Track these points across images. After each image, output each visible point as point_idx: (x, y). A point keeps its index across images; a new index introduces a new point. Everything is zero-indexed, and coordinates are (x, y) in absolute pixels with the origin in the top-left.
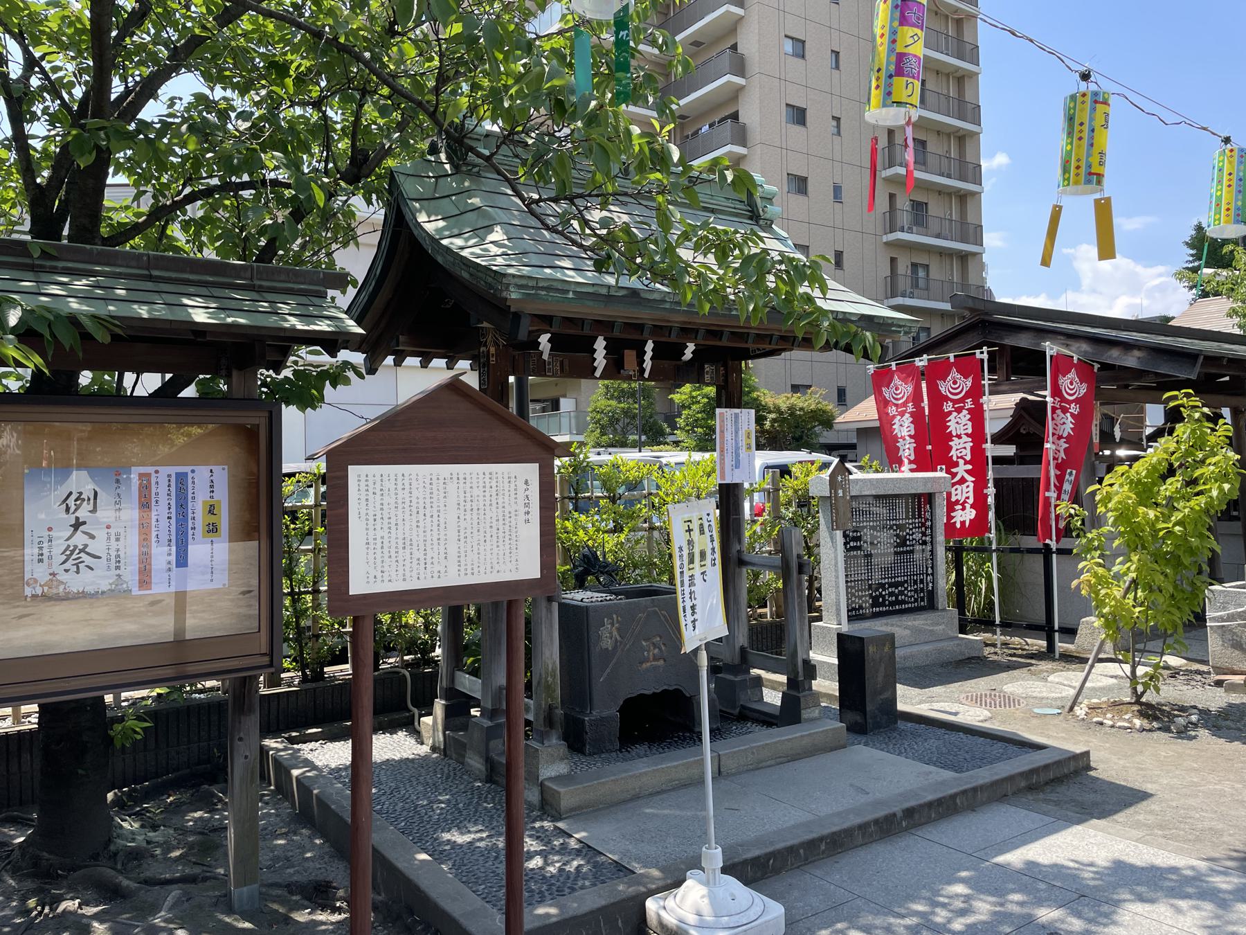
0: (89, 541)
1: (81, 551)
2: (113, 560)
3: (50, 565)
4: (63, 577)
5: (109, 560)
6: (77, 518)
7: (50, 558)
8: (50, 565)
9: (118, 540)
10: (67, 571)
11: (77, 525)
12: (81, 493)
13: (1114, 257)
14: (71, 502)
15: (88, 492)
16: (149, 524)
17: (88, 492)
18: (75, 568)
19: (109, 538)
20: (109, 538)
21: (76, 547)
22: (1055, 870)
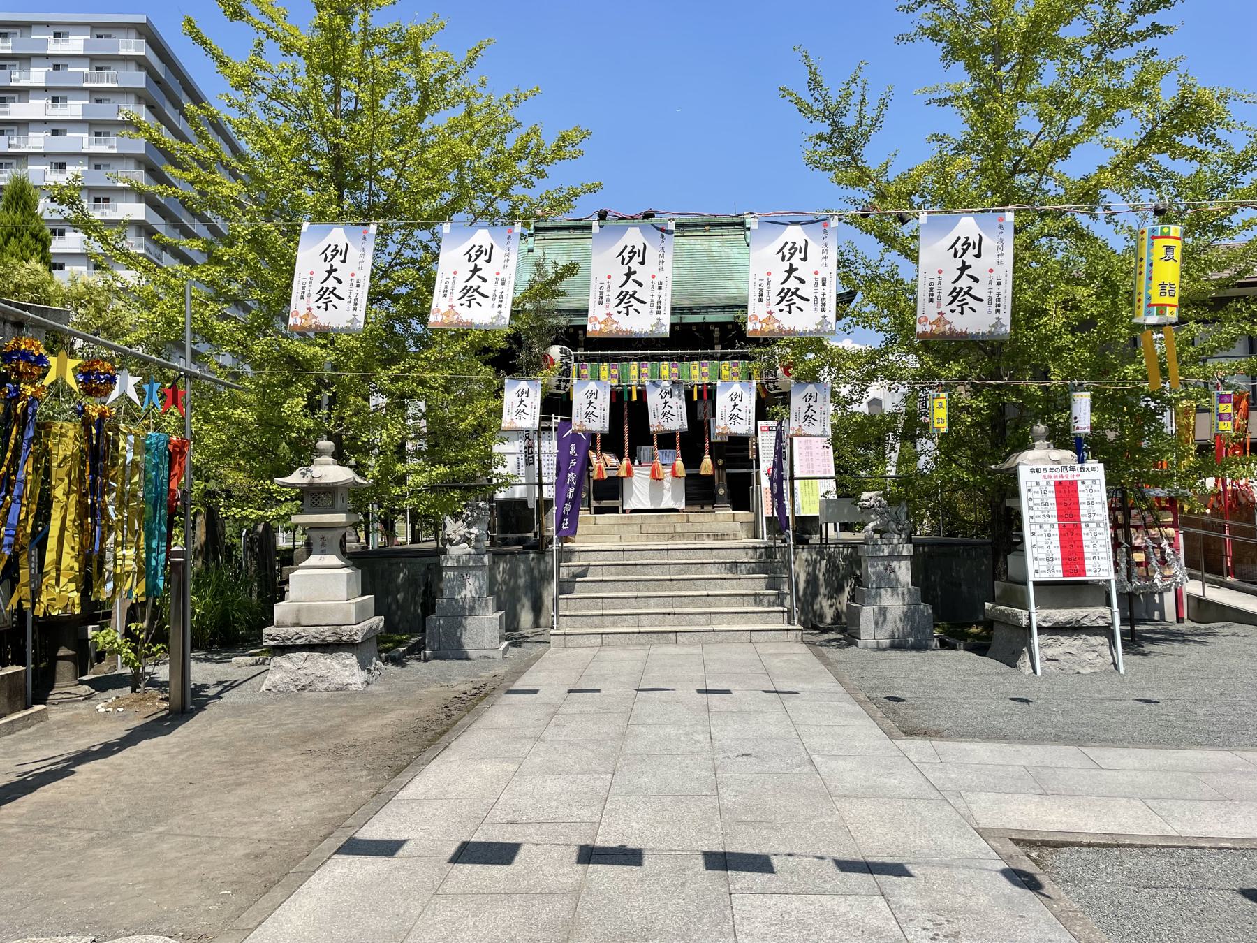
0: (973, 284)
2: (994, 302)
8: (768, 305)
9: (999, 284)
10: (952, 311)
15: (639, 247)
16: (36, 519)
18: (959, 309)
20: (991, 282)
21: (961, 289)
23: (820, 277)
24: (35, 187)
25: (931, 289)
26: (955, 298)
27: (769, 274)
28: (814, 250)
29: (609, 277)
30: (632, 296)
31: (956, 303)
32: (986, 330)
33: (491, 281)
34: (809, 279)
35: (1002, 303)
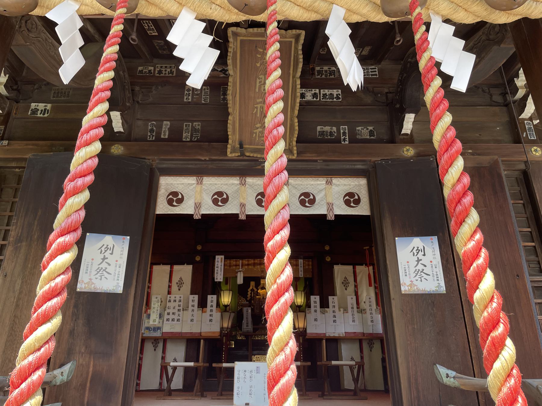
0: (424, 268)
1: (104, 270)
3: (90, 275)
4: (94, 281)
5: (115, 276)
6: (104, 256)
7: (409, 274)
8: (410, 277)
9: (120, 267)
10: (96, 278)
11: (104, 258)
12: (108, 246)
13: (291, 216)
14: (103, 249)
15: (421, 247)
17: (421, 247)
18: (420, 279)
19: (116, 266)
21: (419, 270)
22: (11, 365)
23: (118, 263)
24: (453, 191)
25: (405, 270)
26: (98, 272)
27: (93, 259)
28: (428, 251)
29: (408, 262)
30: (104, 270)
31: (99, 275)
32: (434, 289)
33: (113, 263)
34: (113, 263)
35: (439, 276)
